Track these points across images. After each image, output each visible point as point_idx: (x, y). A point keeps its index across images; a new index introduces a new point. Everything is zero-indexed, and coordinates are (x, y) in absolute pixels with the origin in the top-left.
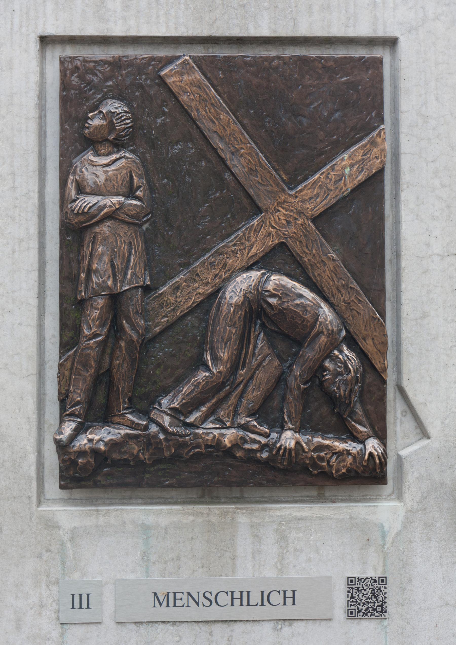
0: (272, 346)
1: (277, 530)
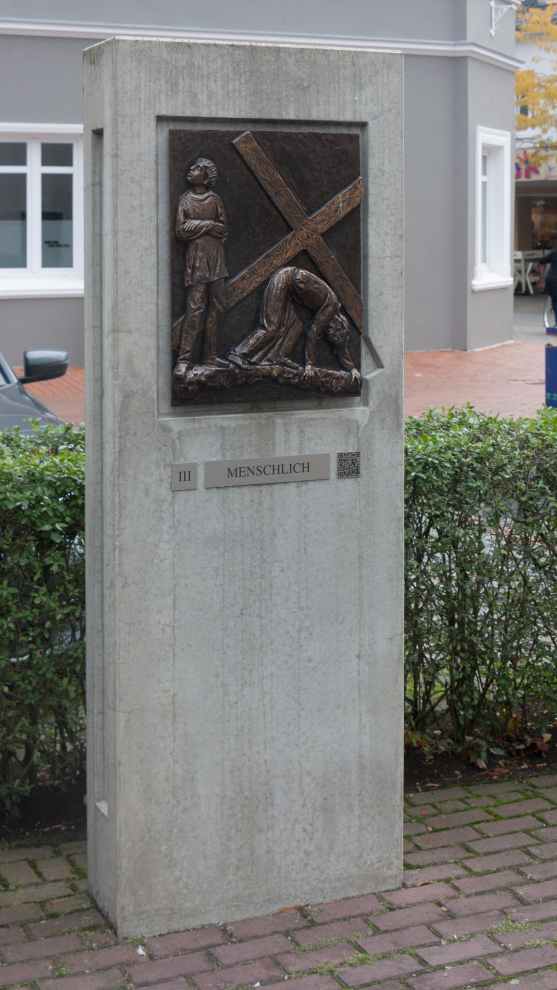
0: (298, 314)
1: (298, 427)
